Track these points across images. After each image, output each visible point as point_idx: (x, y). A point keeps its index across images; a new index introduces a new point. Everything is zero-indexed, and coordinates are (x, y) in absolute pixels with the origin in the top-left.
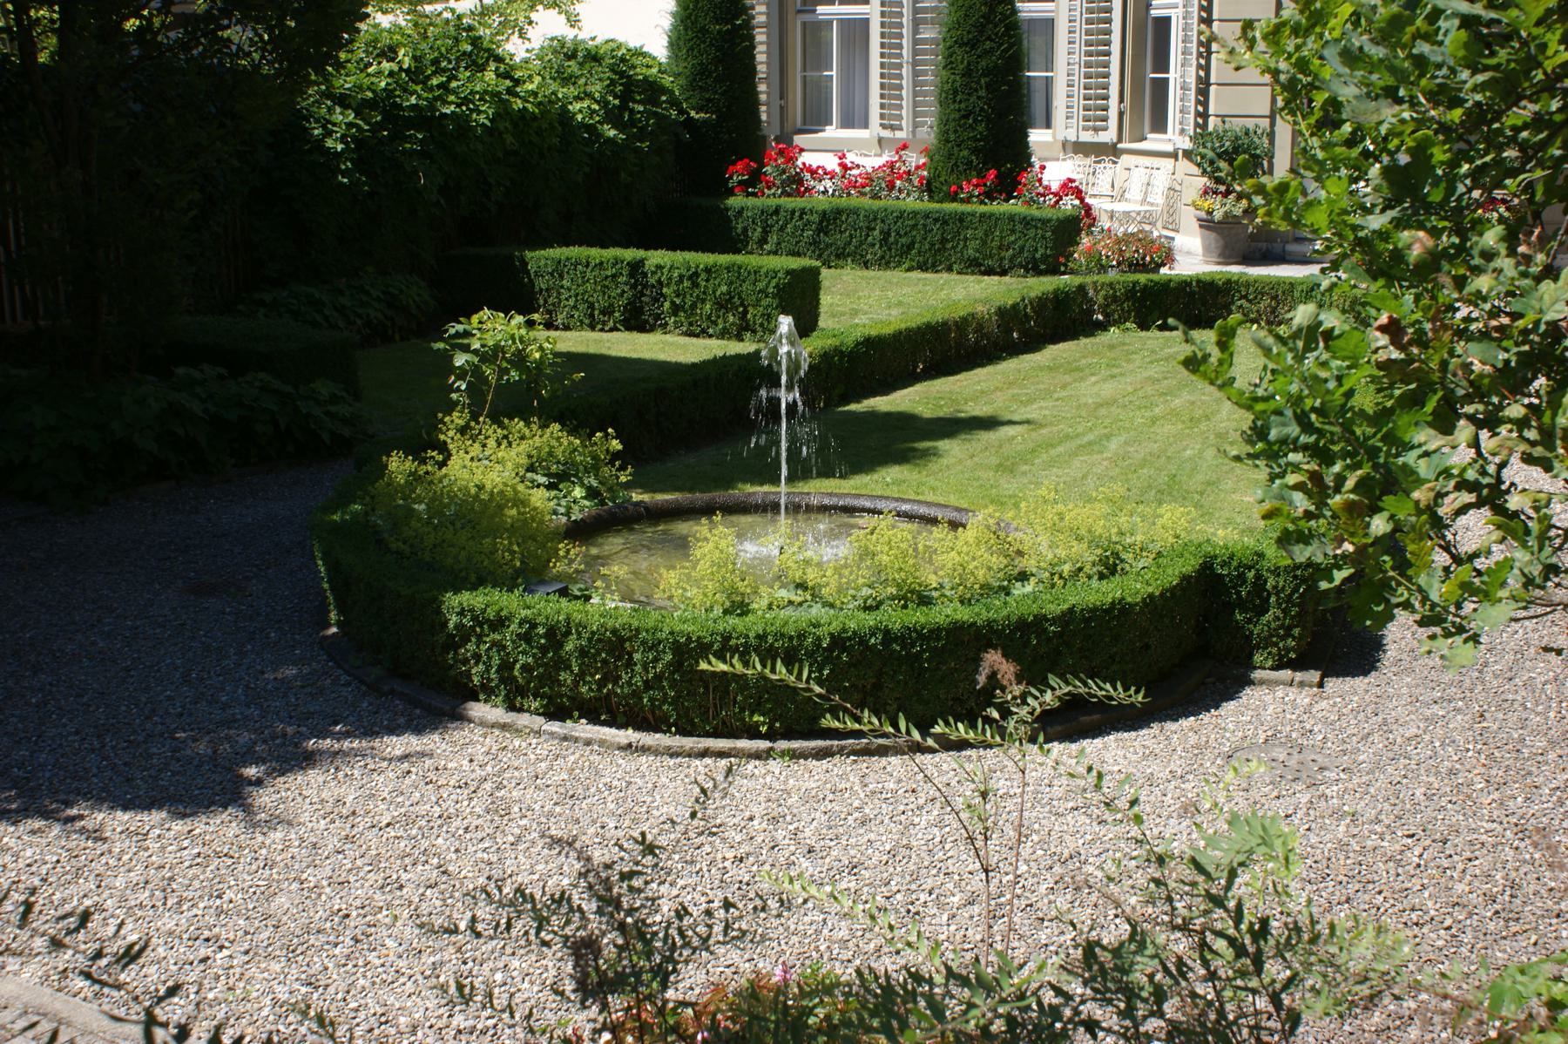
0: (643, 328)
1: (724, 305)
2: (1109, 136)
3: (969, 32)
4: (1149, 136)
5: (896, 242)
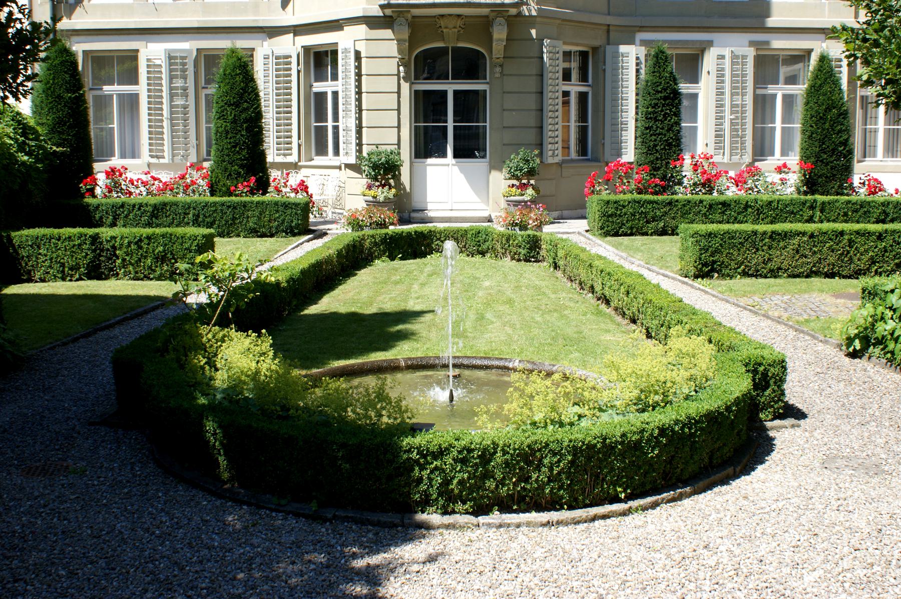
0: (99, 277)
1: (162, 259)
2: (293, 158)
3: (234, 98)
4: (315, 158)
5: (204, 221)
